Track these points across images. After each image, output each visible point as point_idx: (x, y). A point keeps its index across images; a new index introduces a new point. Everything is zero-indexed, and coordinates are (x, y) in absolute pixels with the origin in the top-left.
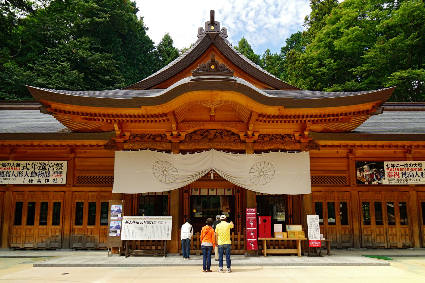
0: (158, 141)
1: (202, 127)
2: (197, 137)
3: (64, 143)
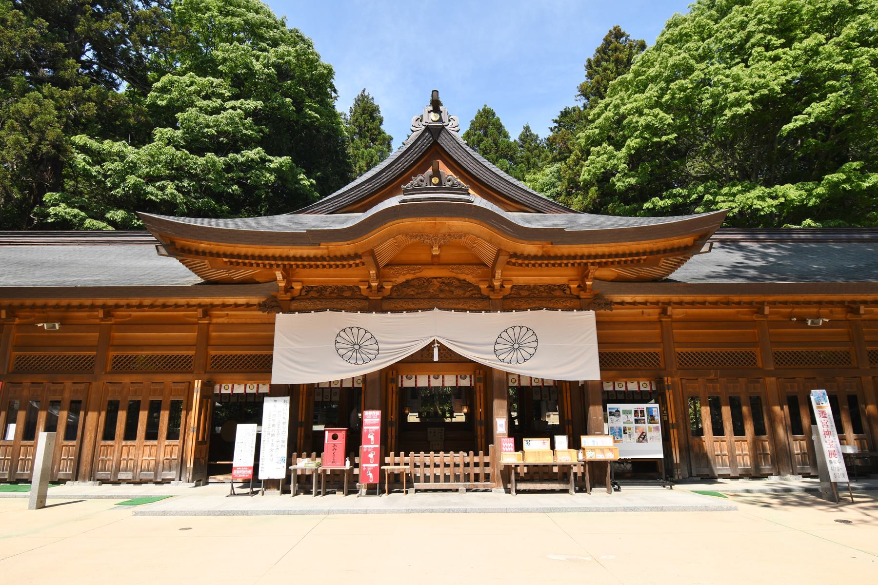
1: (419, 275)
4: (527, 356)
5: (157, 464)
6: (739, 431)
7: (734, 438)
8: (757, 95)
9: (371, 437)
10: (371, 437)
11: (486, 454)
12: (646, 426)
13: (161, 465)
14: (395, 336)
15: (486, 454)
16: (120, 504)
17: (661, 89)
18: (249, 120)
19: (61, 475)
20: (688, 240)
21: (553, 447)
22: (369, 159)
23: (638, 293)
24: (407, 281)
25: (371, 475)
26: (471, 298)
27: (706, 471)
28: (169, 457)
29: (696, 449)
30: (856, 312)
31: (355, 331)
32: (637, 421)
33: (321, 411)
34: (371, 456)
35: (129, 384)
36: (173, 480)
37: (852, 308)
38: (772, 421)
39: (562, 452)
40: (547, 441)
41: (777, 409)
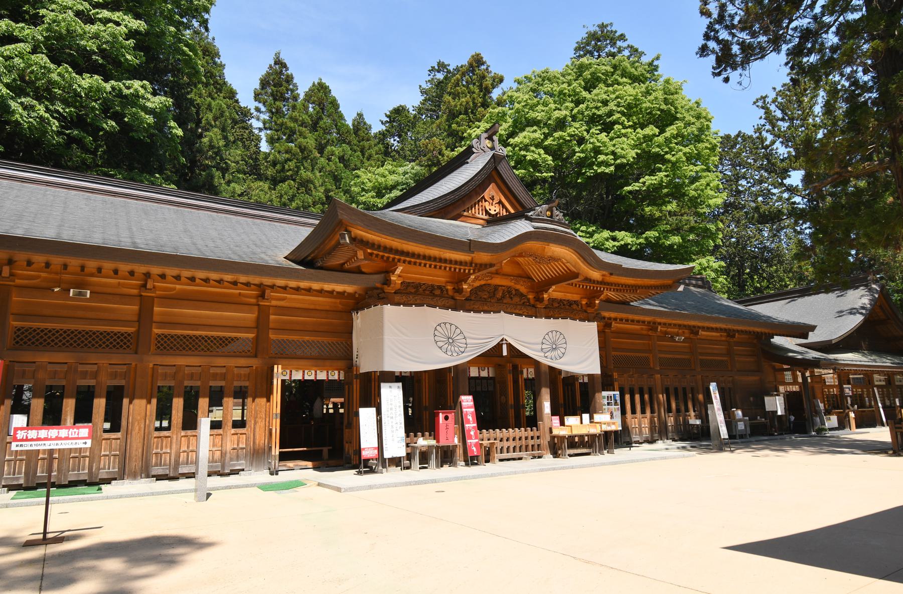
0: (436, 296)
3: (686, 323)
5: (223, 454)
6: (643, 412)
7: (641, 416)
8: (618, 161)
9: (470, 418)
10: (470, 418)
12: (613, 407)
13: (228, 455)
14: (479, 332)
16: (678, 448)
17: (544, 133)
18: (131, 42)
19: (103, 474)
20: (669, 282)
23: (318, 280)
24: (481, 286)
25: (474, 449)
27: (628, 440)
28: (235, 446)
30: (697, 333)
31: (453, 327)
32: (608, 404)
33: (428, 397)
34: (472, 433)
35: (50, 362)
36: (243, 470)
37: (694, 330)
38: (659, 404)
41: (661, 396)
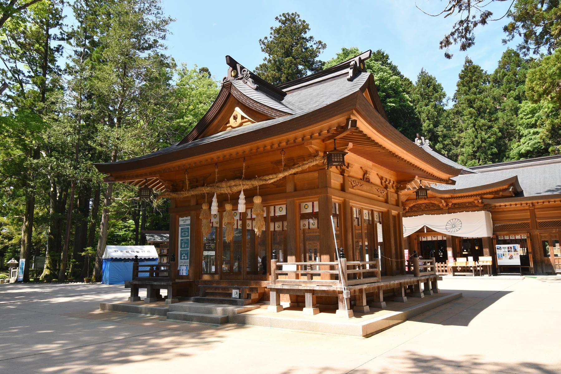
2: (415, 209)
4: (458, 229)
11: (445, 263)
15: (445, 263)
21: (467, 260)
22: (427, 113)
23: (506, 202)
26: (437, 210)
27: (550, 271)
29: (546, 262)
32: (509, 251)
39: (471, 262)
40: (465, 259)
